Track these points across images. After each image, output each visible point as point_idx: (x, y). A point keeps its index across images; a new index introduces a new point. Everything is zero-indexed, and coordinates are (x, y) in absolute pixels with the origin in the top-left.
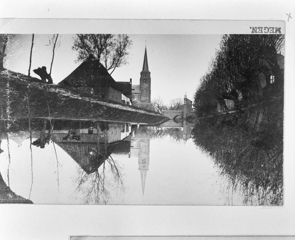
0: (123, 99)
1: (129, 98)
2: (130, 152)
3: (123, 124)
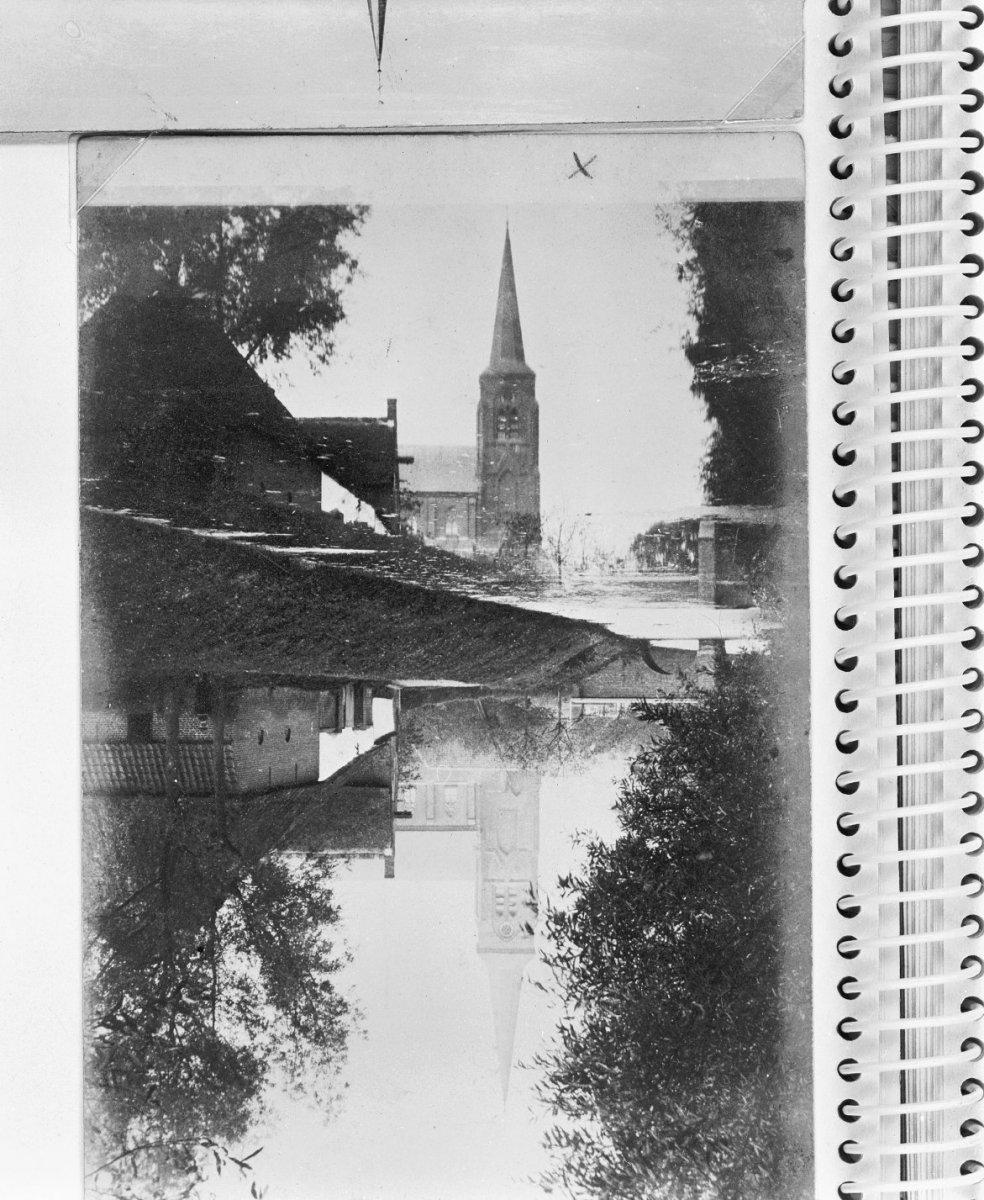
0: (327, 506)
1: (368, 502)
2: (393, 847)
3: (335, 687)
